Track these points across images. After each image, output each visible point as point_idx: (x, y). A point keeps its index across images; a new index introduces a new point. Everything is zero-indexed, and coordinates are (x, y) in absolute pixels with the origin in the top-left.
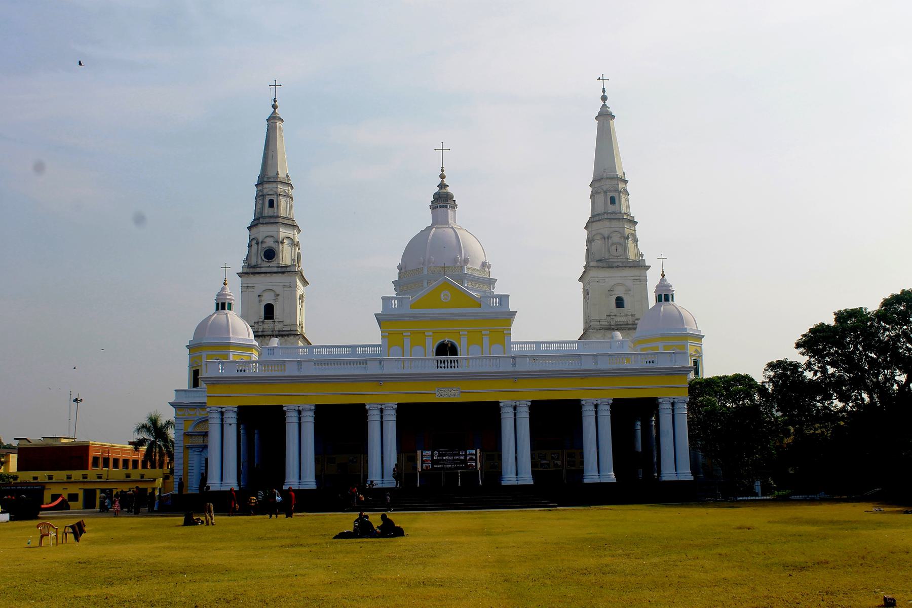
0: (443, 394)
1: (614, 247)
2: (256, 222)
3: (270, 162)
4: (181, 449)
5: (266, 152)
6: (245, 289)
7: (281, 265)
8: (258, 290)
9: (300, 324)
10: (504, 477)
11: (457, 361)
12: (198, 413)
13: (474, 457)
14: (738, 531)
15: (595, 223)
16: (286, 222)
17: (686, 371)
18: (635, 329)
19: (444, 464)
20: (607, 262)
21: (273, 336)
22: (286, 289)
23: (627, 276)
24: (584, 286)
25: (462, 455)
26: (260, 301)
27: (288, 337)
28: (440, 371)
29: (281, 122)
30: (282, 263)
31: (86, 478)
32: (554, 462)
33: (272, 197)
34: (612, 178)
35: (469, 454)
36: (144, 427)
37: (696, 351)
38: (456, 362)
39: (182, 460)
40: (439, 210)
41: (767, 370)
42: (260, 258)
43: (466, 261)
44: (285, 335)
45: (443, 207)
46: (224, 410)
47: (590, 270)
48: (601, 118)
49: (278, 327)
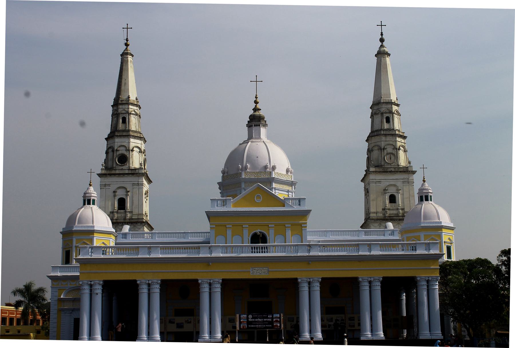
0: (256, 272)
3: (123, 88)
6: (103, 186)
7: (131, 168)
8: (113, 187)
9: (145, 214)
10: (301, 334)
11: (267, 247)
13: (279, 320)
15: (374, 137)
16: (135, 135)
18: (403, 220)
19: (256, 325)
20: (383, 168)
22: (134, 187)
24: (365, 186)
26: (115, 196)
29: (131, 57)
33: (124, 115)
34: (387, 103)
37: (449, 239)
38: (266, 248)
40: (254, 129)
42: (115, 162)
43: (274, 168)
45: (257, 125)
46: (92, 283)
47: (369, 174)
48: (379, 56)
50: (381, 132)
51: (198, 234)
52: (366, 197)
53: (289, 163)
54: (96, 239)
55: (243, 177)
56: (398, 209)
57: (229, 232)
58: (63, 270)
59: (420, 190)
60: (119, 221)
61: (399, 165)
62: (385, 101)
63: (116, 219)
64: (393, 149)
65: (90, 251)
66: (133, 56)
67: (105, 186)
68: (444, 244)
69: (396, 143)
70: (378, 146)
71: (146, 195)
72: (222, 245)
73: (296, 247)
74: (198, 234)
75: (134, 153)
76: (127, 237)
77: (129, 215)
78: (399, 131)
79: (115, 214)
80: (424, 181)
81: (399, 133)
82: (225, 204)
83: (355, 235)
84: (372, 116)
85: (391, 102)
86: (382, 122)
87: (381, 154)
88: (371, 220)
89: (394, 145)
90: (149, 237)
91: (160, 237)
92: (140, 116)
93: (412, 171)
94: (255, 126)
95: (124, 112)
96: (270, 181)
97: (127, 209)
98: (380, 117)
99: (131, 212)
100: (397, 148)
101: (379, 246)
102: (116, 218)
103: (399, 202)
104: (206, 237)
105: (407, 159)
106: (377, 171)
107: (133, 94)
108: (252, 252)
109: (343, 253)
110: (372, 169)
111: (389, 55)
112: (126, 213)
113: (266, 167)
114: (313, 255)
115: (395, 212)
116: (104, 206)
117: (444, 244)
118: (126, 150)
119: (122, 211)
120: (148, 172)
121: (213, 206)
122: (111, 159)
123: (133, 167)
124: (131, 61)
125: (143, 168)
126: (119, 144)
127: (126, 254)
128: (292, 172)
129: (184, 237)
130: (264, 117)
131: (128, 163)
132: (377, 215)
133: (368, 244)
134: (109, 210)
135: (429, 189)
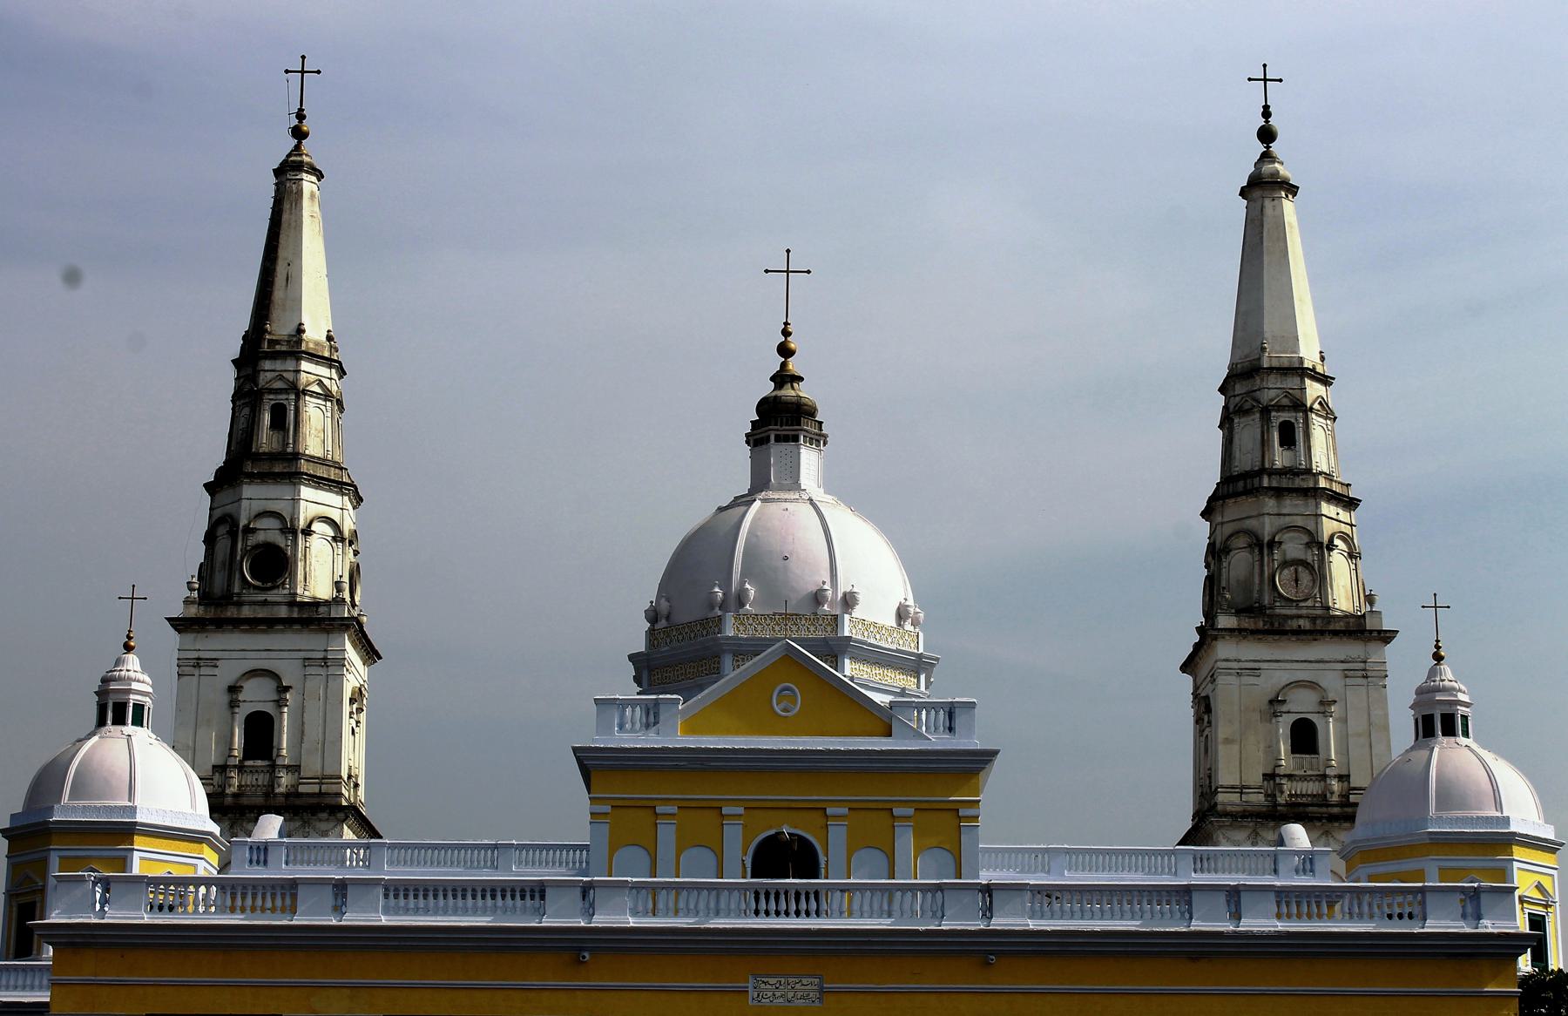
0: (770, 994)
3: (278, 294)
6: (191, 666)
7: (298, 599)
8: (229, 672)
9: (350, 777)
16: (321, 472)
20: (1269, 616)
22: (310, 670)
23: (1326, 658)
24: (1196, 688)
26: (233, 704)
29: (314, 179)
37: (1539, 887)
40: (776, 451)
42: (237, 576)
43: (849, 601)
48: (1257, 193)
50: (1261, 481)
51: (548, 851)
52: (1202, 731)
53: (908, 582)
54: (141, 858)
55: (730, 633)
56: (1324, 777)
57: (667, 834)
58: (20, 982)
59: (1422, 694)
60: (245, 801)
61: (1328, 608)
62: (1275, 364)
63: (234, 795)
64: (1308, 545)
65: (98, 896)
66: (320, 176)
67: (198, 666)
68: (1518, 906)
69: (1318, 524)
70: (1248, 532)
71: (355, 706)
72: (634, 880)
73: (934, 896)
74: (548, 851)
75: (315, 541)
76: (270, 858)
77: (285, 780)
78: (1329, 477)
79: (233, 774)
80: (1438, 658)
81: (1331, 485)
82: (652, 719)
83: (1163, 869)
84: (1227, 422)
85: (1299, 368)
86: (1265, 443)
87: (1262, 565)
88: (1221, 816)
89: (1309, 532)
90: (357, 863)
91: (399, 862)
92: (340, 403)
93: (1380, 632)
94: (778, 439)
95: (279, 385)
96: (836, 649)
97: (278, 756)
98: (1258, 424)
99: (294, 768)
100: (1322, 543)
101: (1272, 896)
102: (234, 790)
103: (1329, 750)
104: (578, 864)
105: (1360, 584)
106: (1245, 630)
107: (316, 321)
108: (757, 913)
109: (1124, 923)
110: (1224, 621)
111: (1292, 190)
112: (274, 771)
113: (817, 598)
114: (1006, 928)
115: (1313, 788)
116: (191, 744)
117: (1518, 906)
118: (281, 529)
119: (259, 763)
120: (365, 618)
121: (603, 727)
122: (224, 564)
123: (307, 593)
124: (312, 196)
125: (348, 599)
126: (258, 506)
127: (243, 910)
128: (917, 619)
129: (493, 863)
130: (815, 409)
131: (290, 581)
132: (1245, 798)
133: (1228, 889)
134: (211, 759)
135: (1460, 690)
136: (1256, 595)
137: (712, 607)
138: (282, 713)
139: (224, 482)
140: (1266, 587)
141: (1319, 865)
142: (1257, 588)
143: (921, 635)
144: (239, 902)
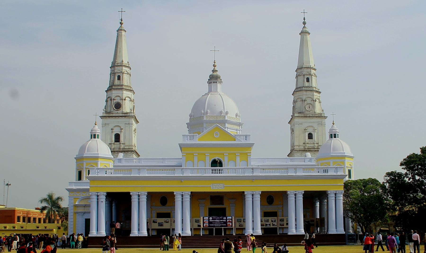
0: (215, 187)
1: (308, 106)
2: (110, 88)
4: (72, 214)
5: (116, 49)
6: (104, 125)
7: (124, 112)
8: (111, 126)
9: (134, 145)
12: (81, 194)
13: (231, 221)
14: (139, 251)
15: (298, 92)
17: (344, 176)
18: (318, 151)
19: (215, 224)
20: (304, 114)
21: (120, 151)
22: (126, 126)
23: (315, 122)
24: (291, 127)
25: (224, 220)
26: (112, 132)
27: (128, 152)
28: (213, 175)
29: (124, 32)
30: (125, 111)
31: (14, 228)
32: (273, 223)
33: (119, 74)
35: (228, 219)
36: (45, 200)
37: (350, 164)
39: (73, 219)
40: (213, 84)
41: (386, 177)
43: (227, 113)
44: (126, 151)
45: (215, 82)
46: (99, 194)
47: (294, 118)
48: (302, 34)
49: (122, 146)
54: (100, 163)
59: (331, 130)
68: (346, 168)
70: (300, 98)
71: (135, 132)
78: (315, 88)
80: (333, 124)
84: (297, 77)
86: (304, 81)
88: (295, 151)
96: (224, 122)
97: (121, 141)
113: (221, 112)
115: (312, 145)
117: (346, 168)
123: (125, 111)
125: (133, 112)
127: (122, 174)
130: (220, 77)
135: (337, 130)
136: (302, 110)
137: (202, 114)
138: (121, 134)
139: (109, 90)
140: (304, 108)
141: (313, 160)
142: (302, 109)
143: (240, 119)
144: (121, 172)
